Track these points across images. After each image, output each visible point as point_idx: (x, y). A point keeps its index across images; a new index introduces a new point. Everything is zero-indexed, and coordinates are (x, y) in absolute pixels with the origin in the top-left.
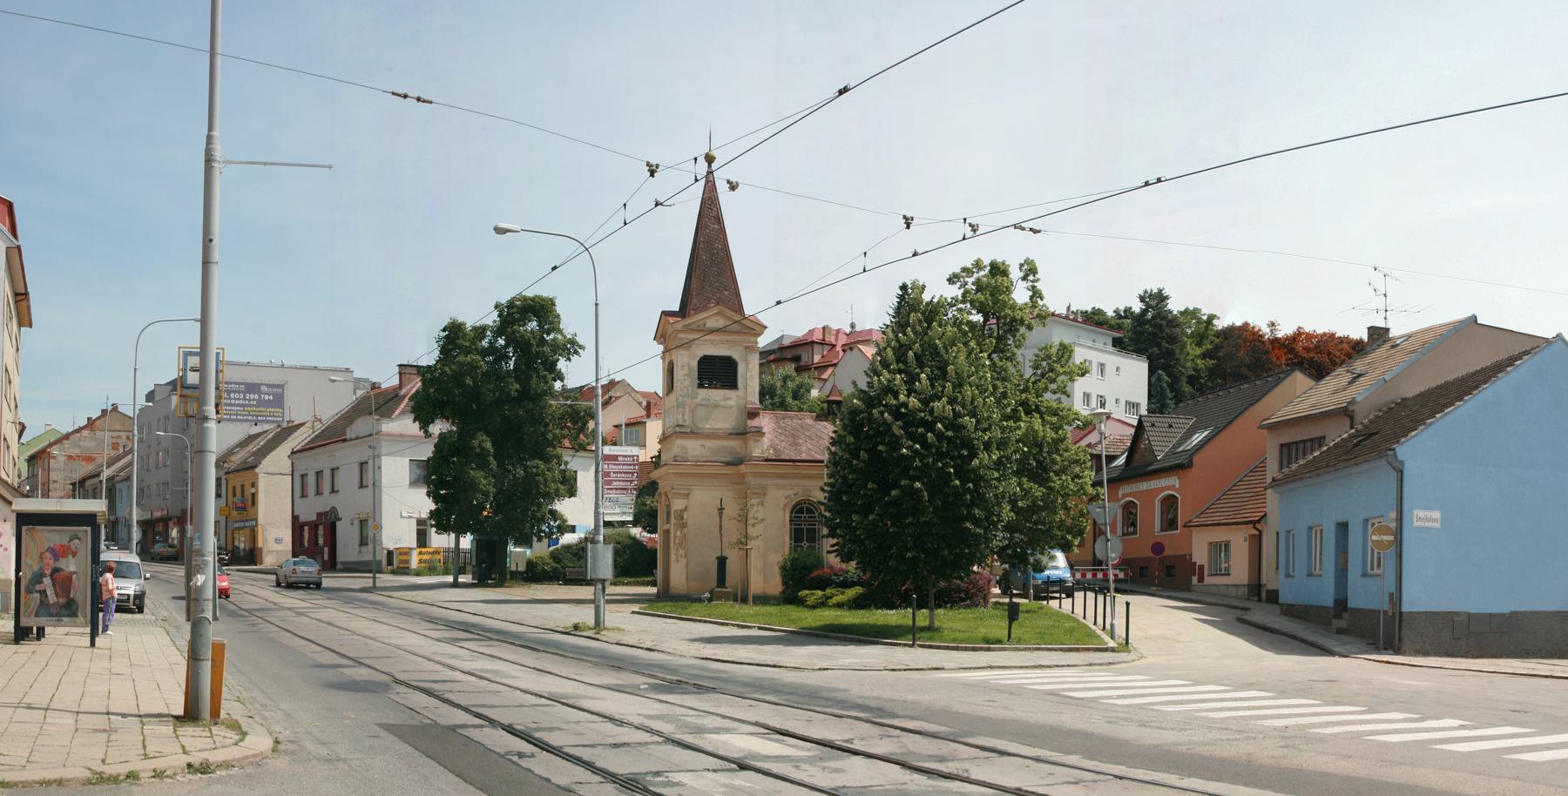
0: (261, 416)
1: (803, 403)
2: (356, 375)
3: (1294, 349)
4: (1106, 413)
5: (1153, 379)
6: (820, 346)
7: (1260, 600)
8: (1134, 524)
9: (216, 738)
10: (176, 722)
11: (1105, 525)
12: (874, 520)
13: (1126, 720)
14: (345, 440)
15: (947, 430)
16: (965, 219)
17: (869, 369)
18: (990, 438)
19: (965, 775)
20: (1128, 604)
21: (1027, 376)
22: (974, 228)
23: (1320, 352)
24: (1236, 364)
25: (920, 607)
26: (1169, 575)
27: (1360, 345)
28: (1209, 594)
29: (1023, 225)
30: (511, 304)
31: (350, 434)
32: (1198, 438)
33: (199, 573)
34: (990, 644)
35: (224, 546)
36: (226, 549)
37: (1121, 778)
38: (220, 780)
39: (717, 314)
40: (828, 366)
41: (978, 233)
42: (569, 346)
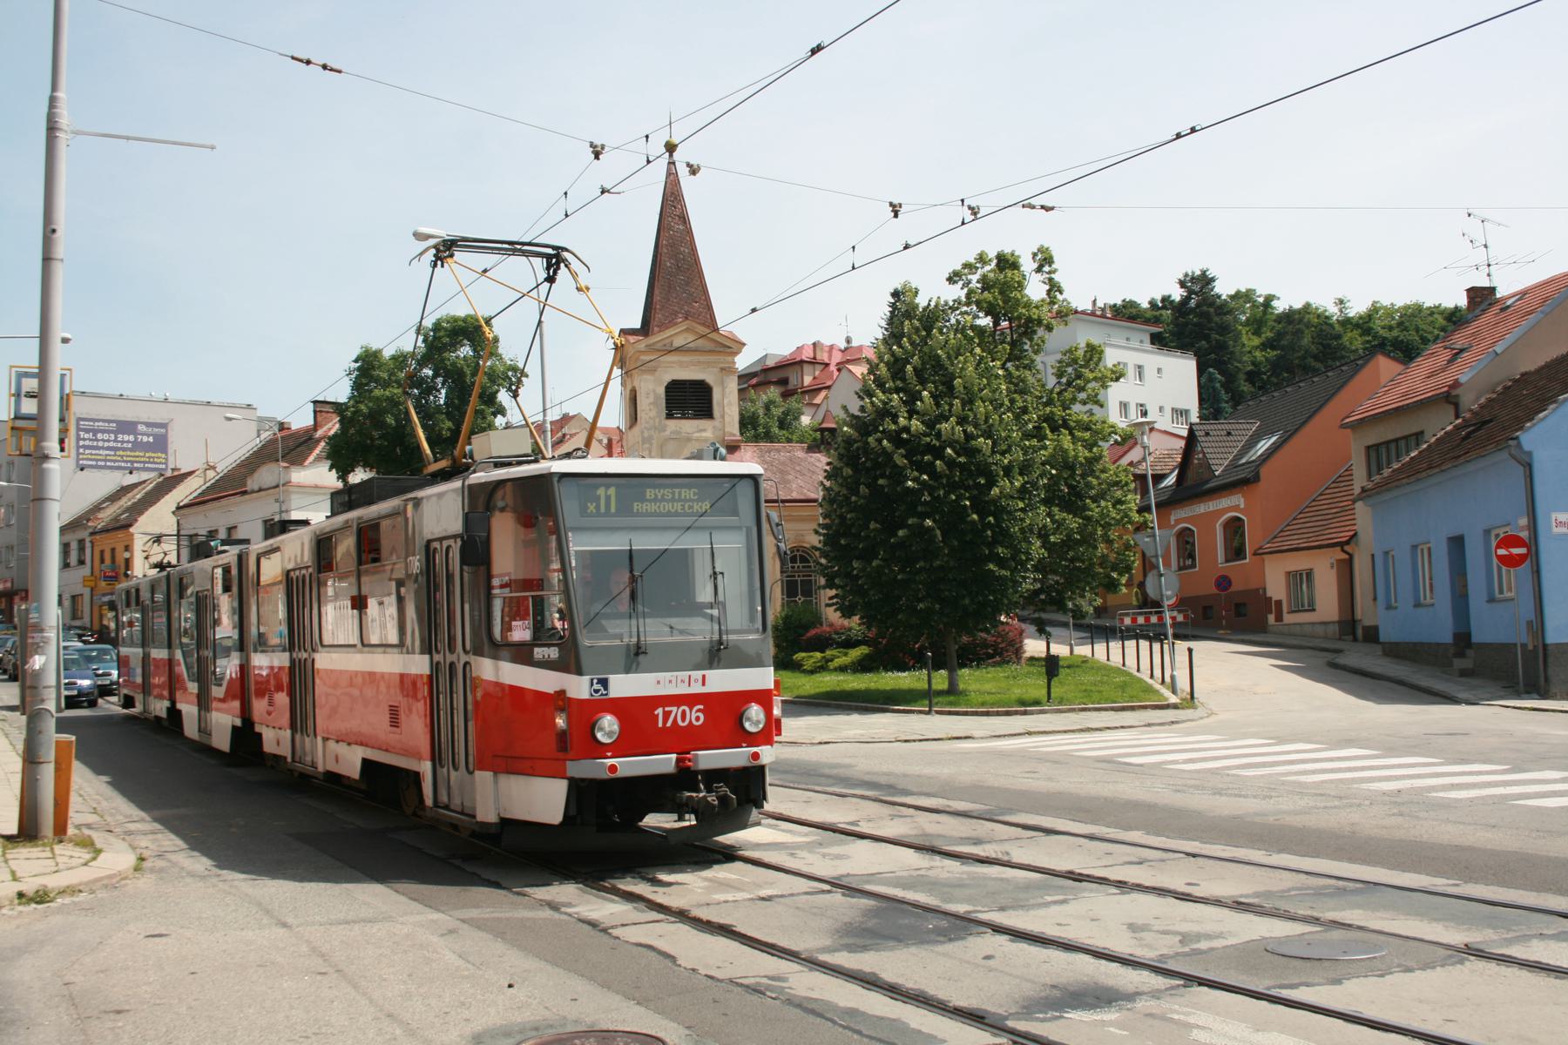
0: (137, 462)
1: (792, 434)
2: (260, 413)
3: (1372, 329)
4: (1148, 423)
5: (1203, 380)
6: (811, 367)
7: (1355, 639)
8: (1192, 556)
9: (59, 859)
10: (6, 843)
11: (1157, 556)
12: (879, 566)
13: (1197, 787)
14: (245, 493)
15: (959, 455)
16: (963, 201)
17: (861, 390)
18: (1010, 462)
19: (1006, 858)
20: (1190, 651)
21: (1049, 386)
22: (974, 211)
23: (1406, 329)
24: (1300, 354)
25: (937, 667)
26: (1238, 614)
27: (1458, 314)
28: (1290, 635)
29: (1033, 201)
30: (437, 326)
31: (252, 484)
32: (1263, 446)
33: (37, 653)
34: (1026, 706)
35: (88, 625)
36: (91, 630)
37: (1194, 856)
38: (60, 910)
39: (687, 330)
40: (820, 389)
41: (979, 216)
42: (510, 373)
